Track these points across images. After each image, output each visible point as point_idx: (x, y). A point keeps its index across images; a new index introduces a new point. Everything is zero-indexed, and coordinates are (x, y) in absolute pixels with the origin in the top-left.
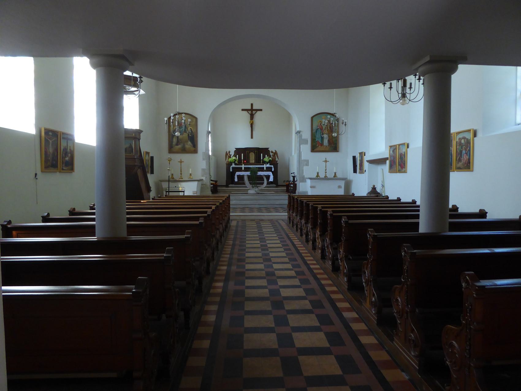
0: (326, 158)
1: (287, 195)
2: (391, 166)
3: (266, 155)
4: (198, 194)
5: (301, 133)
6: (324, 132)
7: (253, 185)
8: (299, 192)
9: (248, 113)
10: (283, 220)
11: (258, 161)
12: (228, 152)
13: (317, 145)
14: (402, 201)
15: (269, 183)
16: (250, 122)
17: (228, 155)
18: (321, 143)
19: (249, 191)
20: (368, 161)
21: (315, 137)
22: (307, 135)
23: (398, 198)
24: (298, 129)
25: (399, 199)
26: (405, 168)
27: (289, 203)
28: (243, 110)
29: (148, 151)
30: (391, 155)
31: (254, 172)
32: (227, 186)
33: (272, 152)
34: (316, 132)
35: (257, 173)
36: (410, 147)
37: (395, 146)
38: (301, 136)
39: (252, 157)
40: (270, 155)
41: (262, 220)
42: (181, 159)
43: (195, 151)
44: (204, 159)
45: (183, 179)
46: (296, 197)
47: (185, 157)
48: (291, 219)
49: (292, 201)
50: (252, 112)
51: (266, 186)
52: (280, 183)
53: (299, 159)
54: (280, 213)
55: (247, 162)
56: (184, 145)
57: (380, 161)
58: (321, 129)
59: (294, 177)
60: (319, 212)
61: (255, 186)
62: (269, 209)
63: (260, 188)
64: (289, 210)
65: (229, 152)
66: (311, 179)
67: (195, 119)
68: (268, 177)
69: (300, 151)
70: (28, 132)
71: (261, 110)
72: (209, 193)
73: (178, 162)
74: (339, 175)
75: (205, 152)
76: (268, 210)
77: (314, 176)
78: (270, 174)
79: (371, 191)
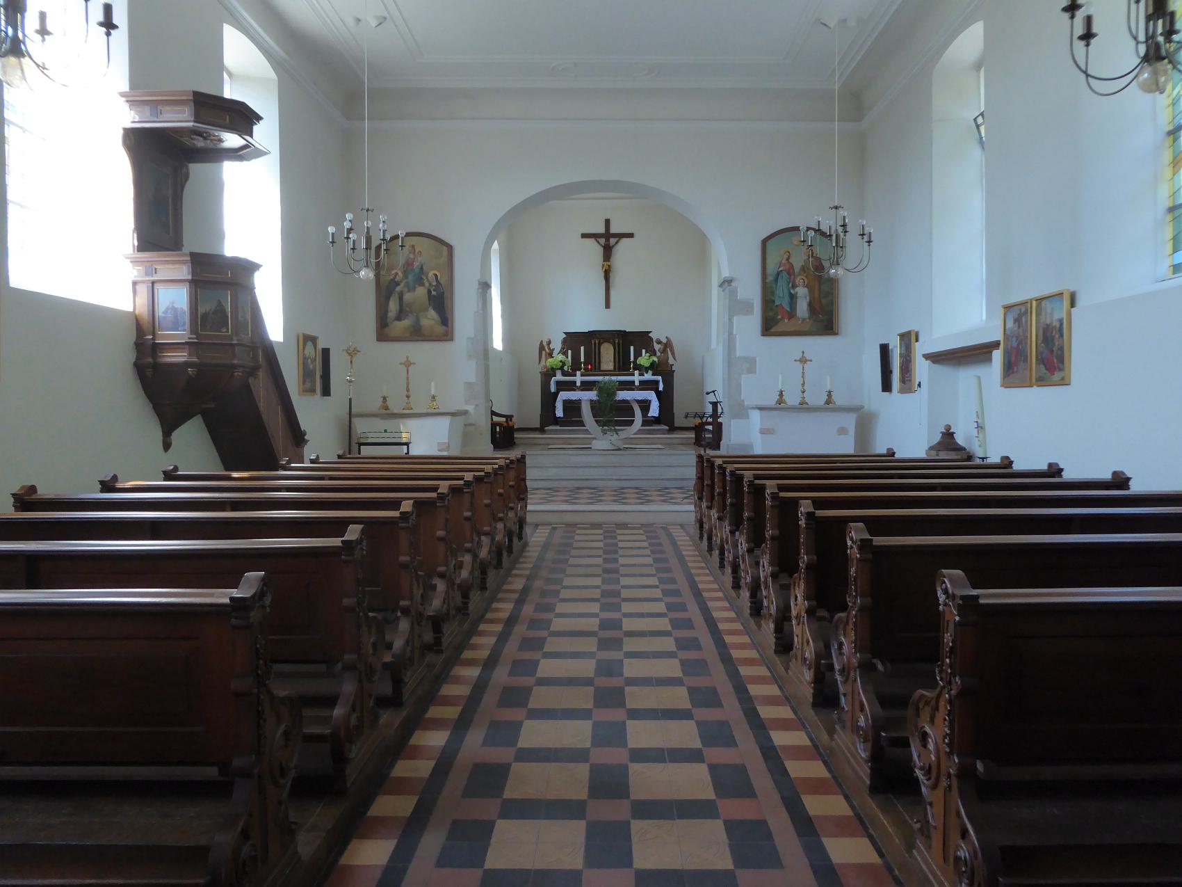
0: (803, 352)
1: (551, 492)
2: (1009, 368)
3: (644, 351)
4: (455, 452)
5: (733, 284)
6: (799, 280)
7: (605, 428)
8: (728, 445)
9: (598, 242)
10: (682, 526)
11: (623, 364)
12: (545, 344)
13: (779, 317)
14: (897, 456)
15: (647, 422)
16: (603, 265)
17: (545, 350)
18: (788, 310)
19: (594, 441)
20: (927, 357)
21: (773, 293)
22: (750, 290)
23: (888, 449)
24: (726, 274)
25: (1007, 463)
26: (1061, 370)
27: (700, 478)
28: (584, 236)
29: (313, 334)
30: (1007, 332)
31: (607, 392)
32: (541, 430)
33: (659, 342)
34: (776, 280)
35: (615, 394)
36: (1080, 302)
37: (1024, 303)
38: (733, 293)
39: (608, 355)
40: (654, 350)
41: (624, 526)
42: (407, 357)
43: (445, 331)
44: (470, 357)
45: (412, 409)
46: (719, 461)
47: (420, 351)
48: (706, 527)
49: (707, 473)
50: (608, 240)
51: (639, 430)
52: (679, 421)
53: (729, 355)
54: (675, 503)
55: (593, 364)
56: (418, 320)
57: (975, 354)
58: (789, 273)
59: (715, 405)
60: (802, 523)
61: (610, 430)
62: (645, 491)
63: (623, 435)
64: (700, 499)
65: (549, 343)
66: (761, 409)
67: (445, 248)
68: (645, 405)
69: (730, 333)
70: (112, 307)
71: (631, 235)
72: (484, 447)
73: (401, 364)
74: (839, 400)
75: (473, 336)
76: (643, 495)
77: (772, 400)
78: (651, 396)
79: (939, 443)
